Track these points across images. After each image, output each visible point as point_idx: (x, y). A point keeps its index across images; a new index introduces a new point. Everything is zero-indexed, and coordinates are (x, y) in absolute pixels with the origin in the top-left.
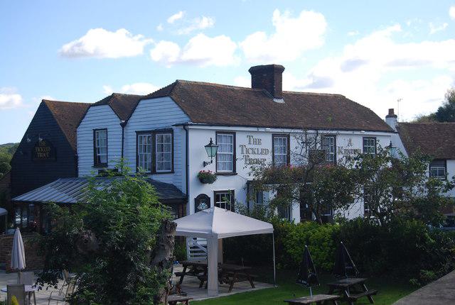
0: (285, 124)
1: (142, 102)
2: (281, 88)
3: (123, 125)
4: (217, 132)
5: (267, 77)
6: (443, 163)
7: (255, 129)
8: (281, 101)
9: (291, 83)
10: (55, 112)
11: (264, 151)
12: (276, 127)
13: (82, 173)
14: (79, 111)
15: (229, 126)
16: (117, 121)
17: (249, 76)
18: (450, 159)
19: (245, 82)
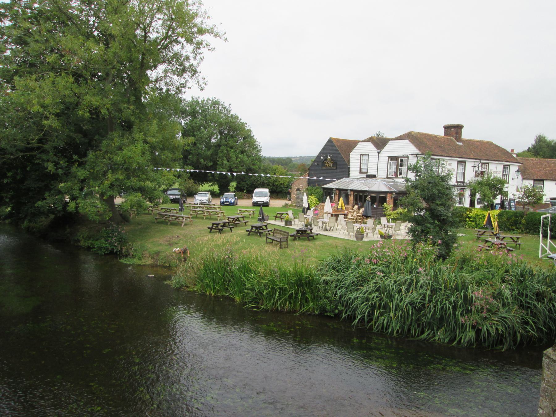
0: (464, 156)
1: (391, 142)
2: (8, 4)
3: (379, 153)
4: (459, 162)
5: (454, 130)
6: (541, 182)
7: (450, 158)
8: (461, 144)
9: (466, 135)
10: (336, 144)
11: (500, 173)
12: (460, 158)
13: (524, 181)
14: (351, 145)
15: (438, 156)
16: (375, 150)
17: (443, 129)
18: (547, 180)
19: (441, 132)
